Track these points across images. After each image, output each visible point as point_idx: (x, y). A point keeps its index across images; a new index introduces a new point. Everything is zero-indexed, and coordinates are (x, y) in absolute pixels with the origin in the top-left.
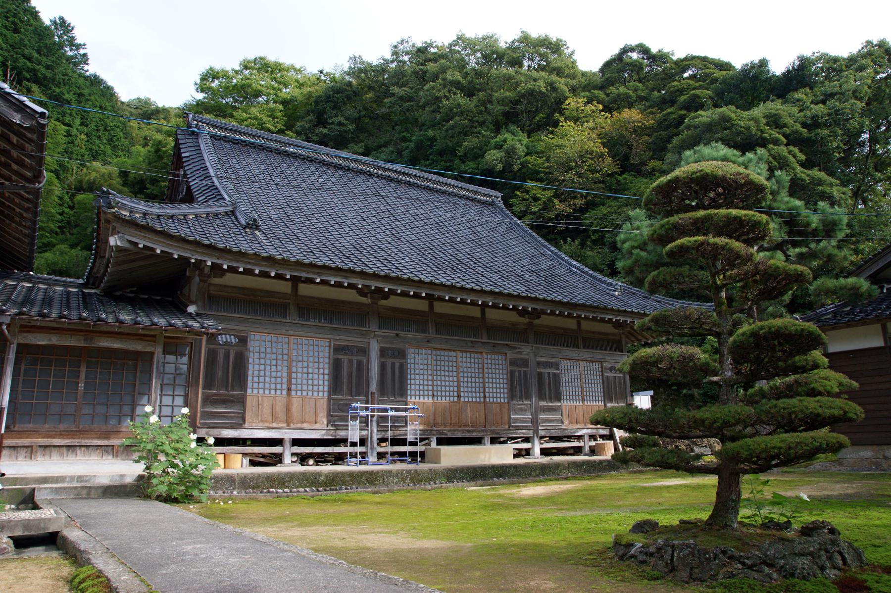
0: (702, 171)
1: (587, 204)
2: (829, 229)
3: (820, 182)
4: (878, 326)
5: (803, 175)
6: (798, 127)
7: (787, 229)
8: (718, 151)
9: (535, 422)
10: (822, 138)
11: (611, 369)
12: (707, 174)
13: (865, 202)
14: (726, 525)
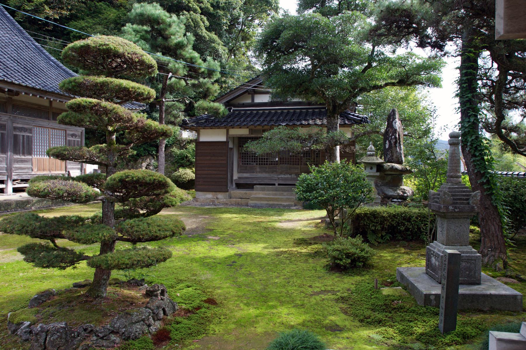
0: (108, 45)
1: (71, 15)
2: (210, 73)
3: (214, 41)
4: (225, 130)
5: (206, 35)
6: (209, 6)
7: (188, 69)
8: (156, 9)
9: (9, 170)
10: (219, 16)
11: (72, 135)
12: (111, 49)
13: (235, 55)
14: (98, 296)
